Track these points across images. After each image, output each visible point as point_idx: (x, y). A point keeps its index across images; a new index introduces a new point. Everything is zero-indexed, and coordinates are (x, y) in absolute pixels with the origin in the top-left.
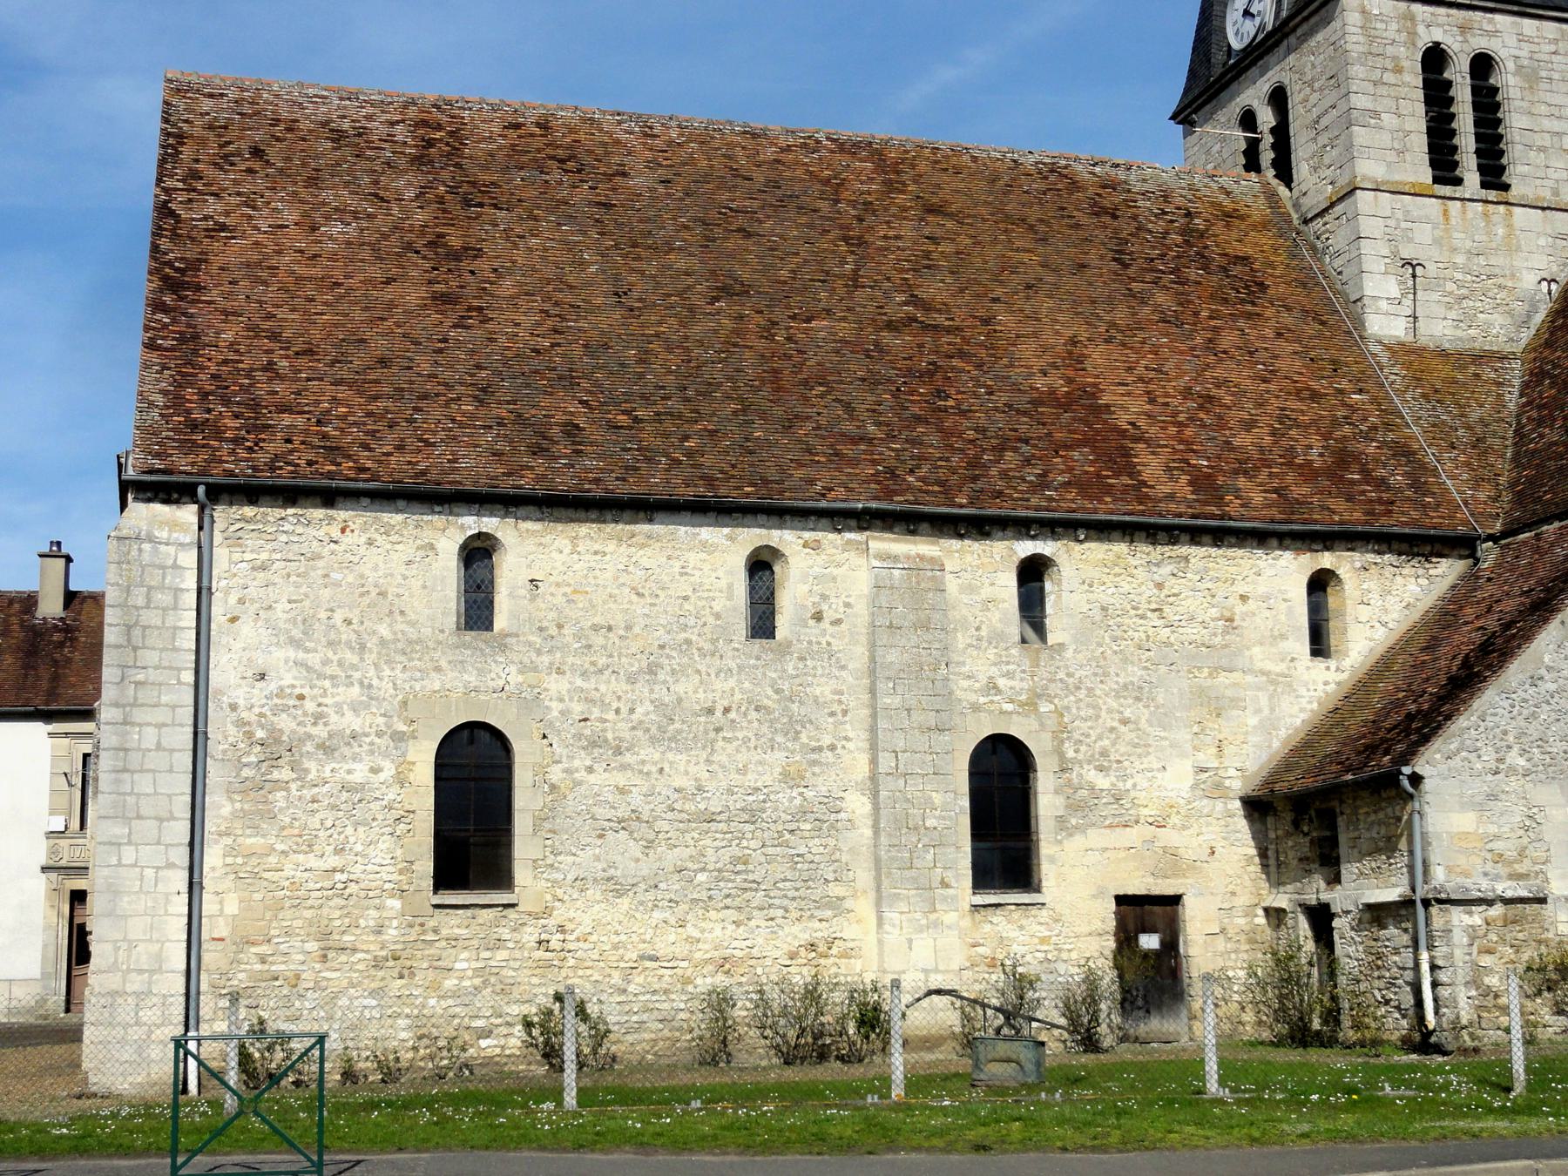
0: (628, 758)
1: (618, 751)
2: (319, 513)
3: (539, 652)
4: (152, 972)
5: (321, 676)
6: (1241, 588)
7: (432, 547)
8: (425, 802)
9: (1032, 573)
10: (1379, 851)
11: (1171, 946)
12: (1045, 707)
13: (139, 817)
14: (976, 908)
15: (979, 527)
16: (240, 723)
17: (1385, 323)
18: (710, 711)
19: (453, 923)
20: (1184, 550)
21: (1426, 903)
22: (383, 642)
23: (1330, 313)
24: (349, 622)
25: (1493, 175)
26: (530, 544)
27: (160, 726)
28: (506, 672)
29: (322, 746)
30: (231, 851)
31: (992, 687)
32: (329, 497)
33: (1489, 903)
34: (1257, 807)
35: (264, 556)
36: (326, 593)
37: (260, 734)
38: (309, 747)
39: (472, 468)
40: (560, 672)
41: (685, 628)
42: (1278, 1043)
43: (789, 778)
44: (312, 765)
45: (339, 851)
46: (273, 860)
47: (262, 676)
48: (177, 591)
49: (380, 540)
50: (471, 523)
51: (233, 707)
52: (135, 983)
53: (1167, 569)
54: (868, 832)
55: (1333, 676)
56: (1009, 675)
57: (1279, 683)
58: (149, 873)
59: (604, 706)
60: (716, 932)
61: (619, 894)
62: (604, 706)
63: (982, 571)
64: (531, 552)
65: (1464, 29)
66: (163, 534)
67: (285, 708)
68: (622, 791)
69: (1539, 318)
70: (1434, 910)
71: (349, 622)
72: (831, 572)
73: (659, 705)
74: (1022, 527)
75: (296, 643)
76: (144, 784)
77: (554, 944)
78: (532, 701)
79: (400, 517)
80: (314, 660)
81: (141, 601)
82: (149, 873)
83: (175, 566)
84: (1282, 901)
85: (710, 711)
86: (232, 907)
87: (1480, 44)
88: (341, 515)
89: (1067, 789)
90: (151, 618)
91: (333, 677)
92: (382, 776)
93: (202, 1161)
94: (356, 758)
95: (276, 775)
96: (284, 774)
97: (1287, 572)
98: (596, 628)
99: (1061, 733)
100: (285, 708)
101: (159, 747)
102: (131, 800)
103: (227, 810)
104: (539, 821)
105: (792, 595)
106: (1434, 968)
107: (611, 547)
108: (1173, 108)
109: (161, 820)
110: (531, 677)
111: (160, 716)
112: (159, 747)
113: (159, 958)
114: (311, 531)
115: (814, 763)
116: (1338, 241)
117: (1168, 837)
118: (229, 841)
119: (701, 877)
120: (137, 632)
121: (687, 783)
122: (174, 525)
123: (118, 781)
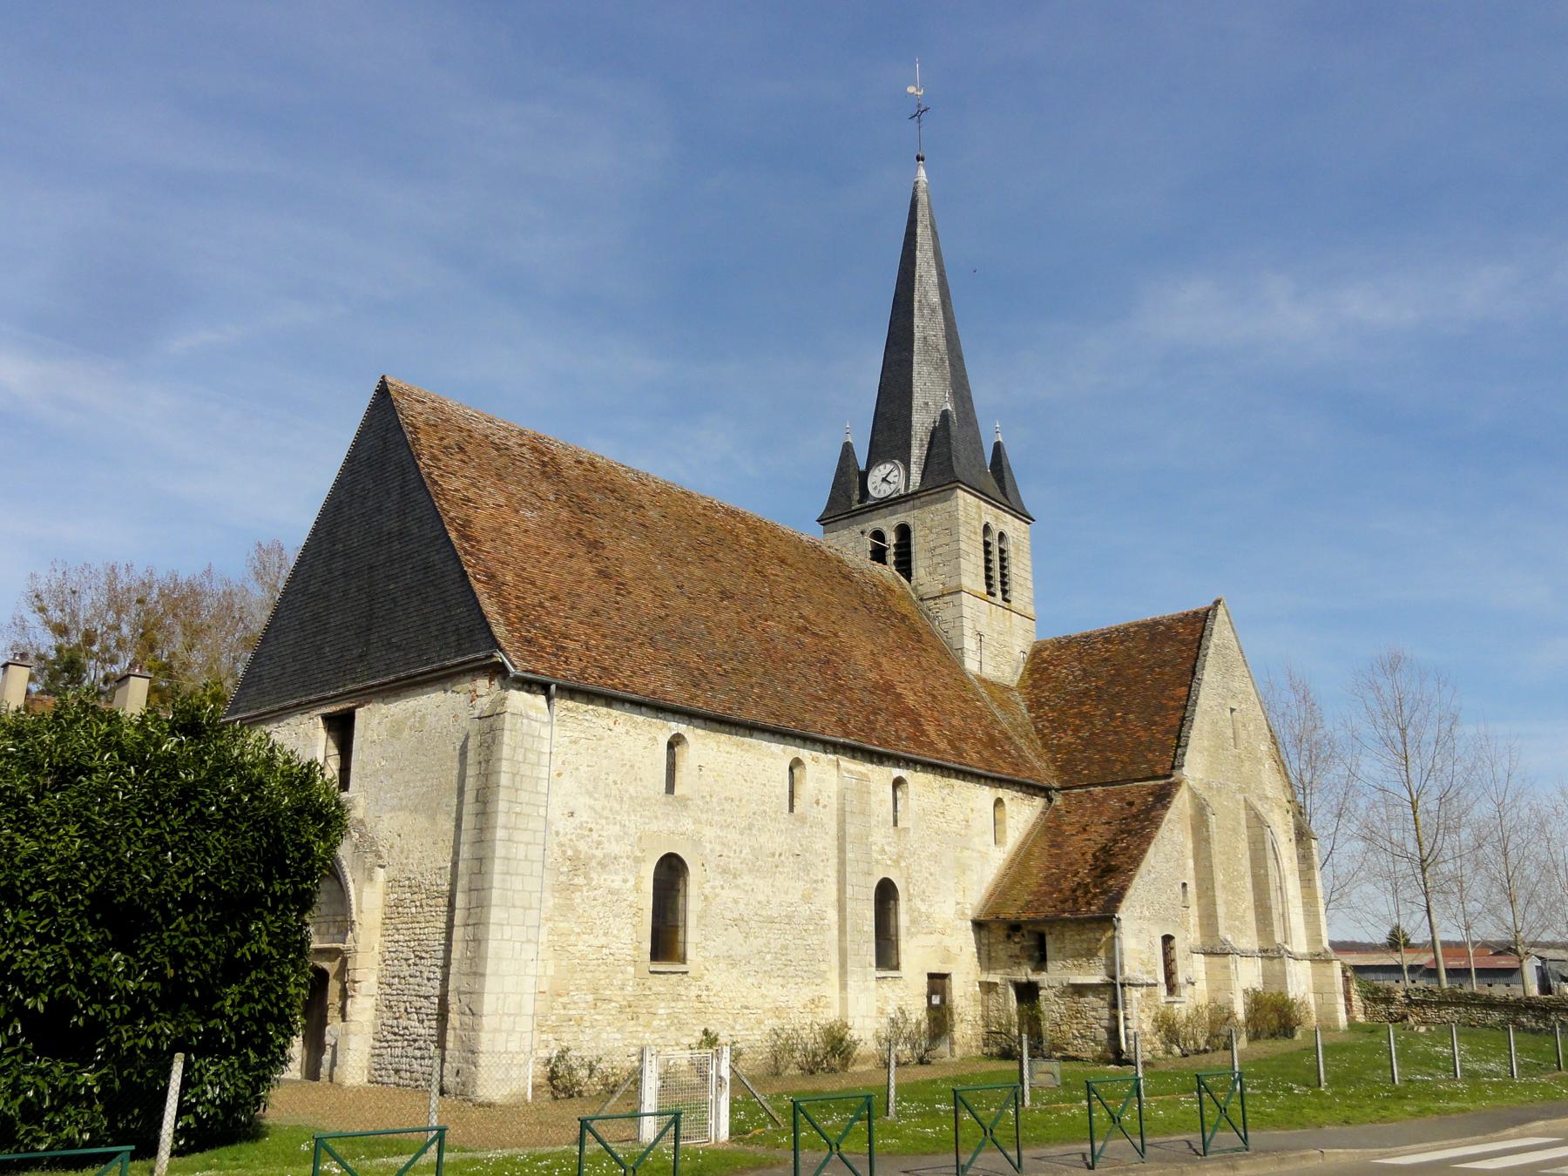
0: (739, 881)
2: (603, 710)
4: (515, 1015)
5: (601, 817)
6: (971, 805)
9: (898, 783)
10: (1081, 956)
11: (943, 1001)
12: (903, 864)
14: (878, 978)
15: (879, 758)
16: (561, 845)
17: (971, 665)
18: (773, 855)
19: (658, 983)
20: (953, 781)
21: (1123, 985)
22: (631, 798)
23: (950, 658)
27: (528, 844)
28: (687, 824)
29: (600, 863)
30: (552, 932)
31: (883, 851)
32: (610, 700)
33: (1142, 985)
34: (978, 925)
35: (576, 735)
36: (605, 762)
37: (570, 853)
38: (594, 863)
39: (675, 695)
41: (764, 803)
42: (990, 1056)
43: (806, 898)
44: (594, 875)
45: (605, 934)
46: (573, 938)
48: (540, 753)
49: (632, 731)
51: (557, 834)
53: (947, 791)
54: (836, 932)
57: (984, 856)
58: (518, 945)
59: (730, 848)
60: (775, 992)
61: (733, 966)
64: (703, 746)
65: (997, 518)
66: (532, 714)
67: (583, 837)
68: (736, 902)
69: (1021, 670)
70: (1126, 989)
72: (825, 773)
73: (753, 849)
75: (590, 794)
76: (516, 883)
77: (704, 998)
78: (697, 843)
79: (641, 718)
84: (995, 978)
85: (773, 855)
86: (551, 972)
87: (1002, 528)
88: (615, 713)
89: (910, 910)
94: (616, 873)
95: (576, 881)
96: (580, 880)
97: (984, 795)
98: (726, 799)
99: (908, 878)
100: (583, 837)
102: (510, 894)
103: (550, 904)
104: (700, 918)
105: (806, 790)
106: (1126, 1019)
109: (525, 908)
114: (599, 721)
116: (947, 614)
117: (947, 941)
118: (550, 924)
119: (768, 957)
120: (518, 778)
121: (762, 898)
122: (533, 706)
123: (504, 880)
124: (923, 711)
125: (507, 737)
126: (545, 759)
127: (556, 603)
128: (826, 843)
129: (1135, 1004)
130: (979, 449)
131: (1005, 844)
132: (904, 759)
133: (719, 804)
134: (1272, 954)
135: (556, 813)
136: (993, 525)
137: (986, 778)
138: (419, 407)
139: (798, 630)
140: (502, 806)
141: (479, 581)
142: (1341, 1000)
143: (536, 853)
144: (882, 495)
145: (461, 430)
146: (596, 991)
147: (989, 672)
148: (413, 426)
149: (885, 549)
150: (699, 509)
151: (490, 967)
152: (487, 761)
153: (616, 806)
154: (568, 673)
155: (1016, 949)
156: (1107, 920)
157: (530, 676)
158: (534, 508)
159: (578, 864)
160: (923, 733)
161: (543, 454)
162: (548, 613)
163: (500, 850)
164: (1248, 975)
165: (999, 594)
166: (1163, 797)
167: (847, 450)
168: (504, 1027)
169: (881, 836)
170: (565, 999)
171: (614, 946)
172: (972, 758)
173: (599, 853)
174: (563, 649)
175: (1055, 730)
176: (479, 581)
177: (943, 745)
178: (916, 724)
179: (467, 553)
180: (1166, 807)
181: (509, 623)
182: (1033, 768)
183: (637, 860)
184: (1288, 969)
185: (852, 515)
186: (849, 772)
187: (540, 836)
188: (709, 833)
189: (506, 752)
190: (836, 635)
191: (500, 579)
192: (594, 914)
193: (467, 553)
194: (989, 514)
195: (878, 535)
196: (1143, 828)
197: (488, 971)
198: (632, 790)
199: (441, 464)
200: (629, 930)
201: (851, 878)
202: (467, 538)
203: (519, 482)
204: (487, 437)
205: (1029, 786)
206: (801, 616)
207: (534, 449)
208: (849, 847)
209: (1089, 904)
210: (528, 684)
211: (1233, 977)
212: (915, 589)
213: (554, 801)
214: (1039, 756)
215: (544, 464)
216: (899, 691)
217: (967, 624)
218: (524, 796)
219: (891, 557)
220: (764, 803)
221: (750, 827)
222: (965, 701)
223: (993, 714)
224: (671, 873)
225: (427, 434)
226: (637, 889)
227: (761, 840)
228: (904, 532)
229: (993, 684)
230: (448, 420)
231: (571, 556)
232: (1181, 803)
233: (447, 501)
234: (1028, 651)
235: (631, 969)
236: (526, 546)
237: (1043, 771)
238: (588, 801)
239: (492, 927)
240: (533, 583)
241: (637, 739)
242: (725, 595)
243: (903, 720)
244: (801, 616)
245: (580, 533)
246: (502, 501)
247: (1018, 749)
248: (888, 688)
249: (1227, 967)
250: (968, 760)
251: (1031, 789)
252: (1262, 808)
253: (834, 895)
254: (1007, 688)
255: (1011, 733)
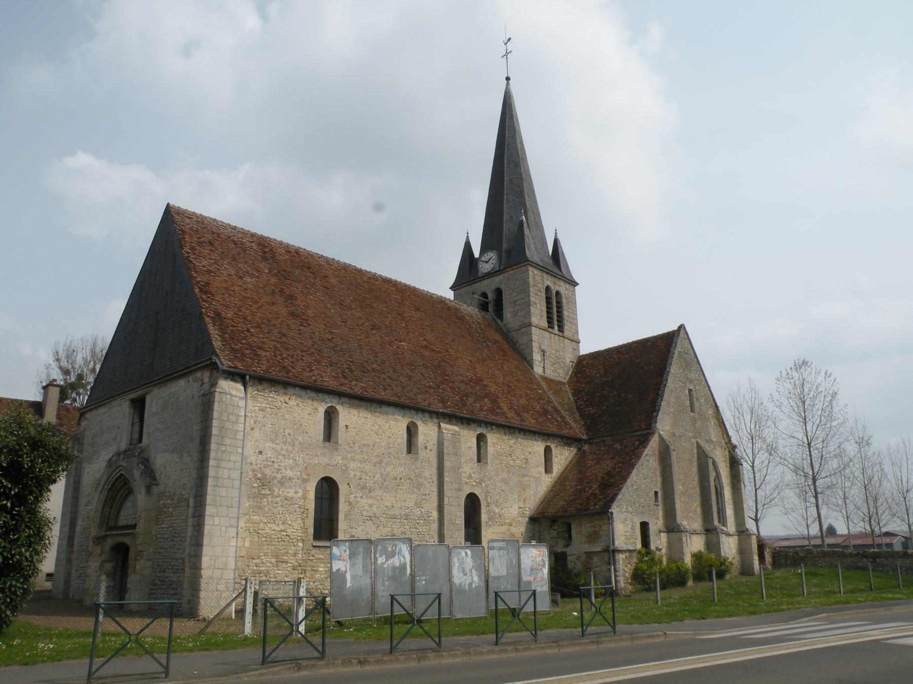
0: (373, 494)
1: (370, 492)
3: (348, 452)
6: (530, 450)
7: (316, 409)
8: (311, 506)
13: (221, 505)
17: (538, 369)
19: (320, 554)
24: (289, 434)
25: (561, 328)
26: (347, 411)
28: (338, 459)
31: (470, 477)
35: (264, 405)
36: (282, 422)
37: (259, 475)
38: (275, 482)
39: (332, 384)
40: (354, 460)
41: (389, 448)
43: (418, 505)
46: (262, 525)
47: (261, 453)
48: (238, 416)
50: (332, 402)
51: (251, 464)
52: (217, 574)
53: (513, 441)
55: (549, 480)
56: (474, 473)
57: (538, 480)
59: (366, 474)
62: (366, 474)
63: (468, 437)
64: (350, 418)
65: (554, 283)
66: (234, 392)
68: (370, 506)
71: (289, 434)
72: (427, 431)
74: (479, 422)
75: (273, 441)
78: (345, 470)
80: (278, 447)
81: (225, 419)
82: (223, 528)
83: (238, 406)
86: (247, 544)
87: (558, 288)
90: (229, 425)
91: (284, 455)
92: (299, 495)
93: (112, 668)
94: (291, 487)
95: (263, 492)
97: (538, 447)
98: (364, 445)
101: (229, 478)
102: (218, 498)
103: (247, 505)
104: (346, 515)
107: (369, 416)
108: (172, 203)
110: (345, 462)
111: (230, 465)
112: (229, 478)
113: (226, 564)
115: (424, 499)
118: (247, 517)
120: (223, 431)
121: (388, 504)
123: (214, 490)
124: (500, 396)
125: (216, 406)
126: (242, 419)
127: (258, 330)
128: (430, 472)
129: (621, 562)
130: (545, 243)
131: (552, 472)
132: (484, 422)
133: (359, 448)
134: (710, 531)
135: (250, 451)
136: (552, 286)
137: (539, 434)
138: (188, 221)
139: (422, 347)
140: (213, 446)
141: (209, 316)
142: (756, 558)
143: (236, 474)
144: (486, 271)
145: (213, 233)
146: (277, 556)
147: (550, 374)
148: (182, 231)
149: (487, 303)
150: (365, 278)
151: (206, 540)
152: (206, 421)
153: (290, 448)
154: (259, 369)
155: (554, 533)
156: (604, 514)
157: (232, 370)
158: (252, 276)
159: (264, 482)
160: (499, 407)
161: (266, 247)
162: (252, 335)
163: (212, 472)
164: (695, 544)
165: (556, 328)
166: (644, 441)
167: (468, 247)
168: (215, 576)
169: (469, 468)
170: (257, 561)
171: (289, 531)
172: (530, 422)
173: (279, 476)
174: (258, 355)
175: (587, 406)
176: (209, 316)
177: (511, 415)
178: (495, 401)
179: (203, 300)
180: (645, 447)
181: (224, 340)
182: (571, 428)
183: (305, 481)
184: (721, 540)
185: (470, 282)
186: (446, 429)
187: (238, 465)
188: (353, 465)
189: (216, 414)
190: (447, 351)
191: (223, 315)
192: (276, 511)
193: (203, 300)
194: (549, 281)
195: (484, 295)
196: (631, 460)
197: (205, 543)
198: (300, 440)
199: (196, 252)
200: (300, 521)
201: (447, 492)
202: (206, 293)
203: (246, 262)
204: (230, 237)
205: (567, 438)
206: (425, 340)
207: (260, 244)
208: (446, 474)
209: (595, 505)
210: (233, 375)
211: (684, 545)
212: (505, 326)
213: (249, 444)
214: (576, 422)
215: (265, 253)
216: (485, 383)
217: (535, 345)
218: (228, 441)
219: (491, 308)
220: (389, 448)
221: (380, 462)
222: (531, 390)
223: (549, 397)
224: (328, 491)
225: (191, 235)
226: (304, 497)
227: (388, 469)
228: (499, 292)
229: (551, 380)
230: (205, 228)
231: (273, 304)
232: (654, 442)
233: (196, 272)
234: (575, 361)
235: (301, 544)
236: (244, 297)
237: (576, 428)
238: (270, 444)
239: (207, 518)
240: (245, 319)
241: (307, 413)
242: (374, 327)
243: (486, 400)
244: (425, 340)
245: (282, 291)
246: (233, 272)
247: (562, 417)
248: (479, 381)
249: (681, 539)
250: (527, 423)
251: (568, 440)
252: (707, 447)
253: (435, 504)
254: (560, 383)
255: (559, 408)
